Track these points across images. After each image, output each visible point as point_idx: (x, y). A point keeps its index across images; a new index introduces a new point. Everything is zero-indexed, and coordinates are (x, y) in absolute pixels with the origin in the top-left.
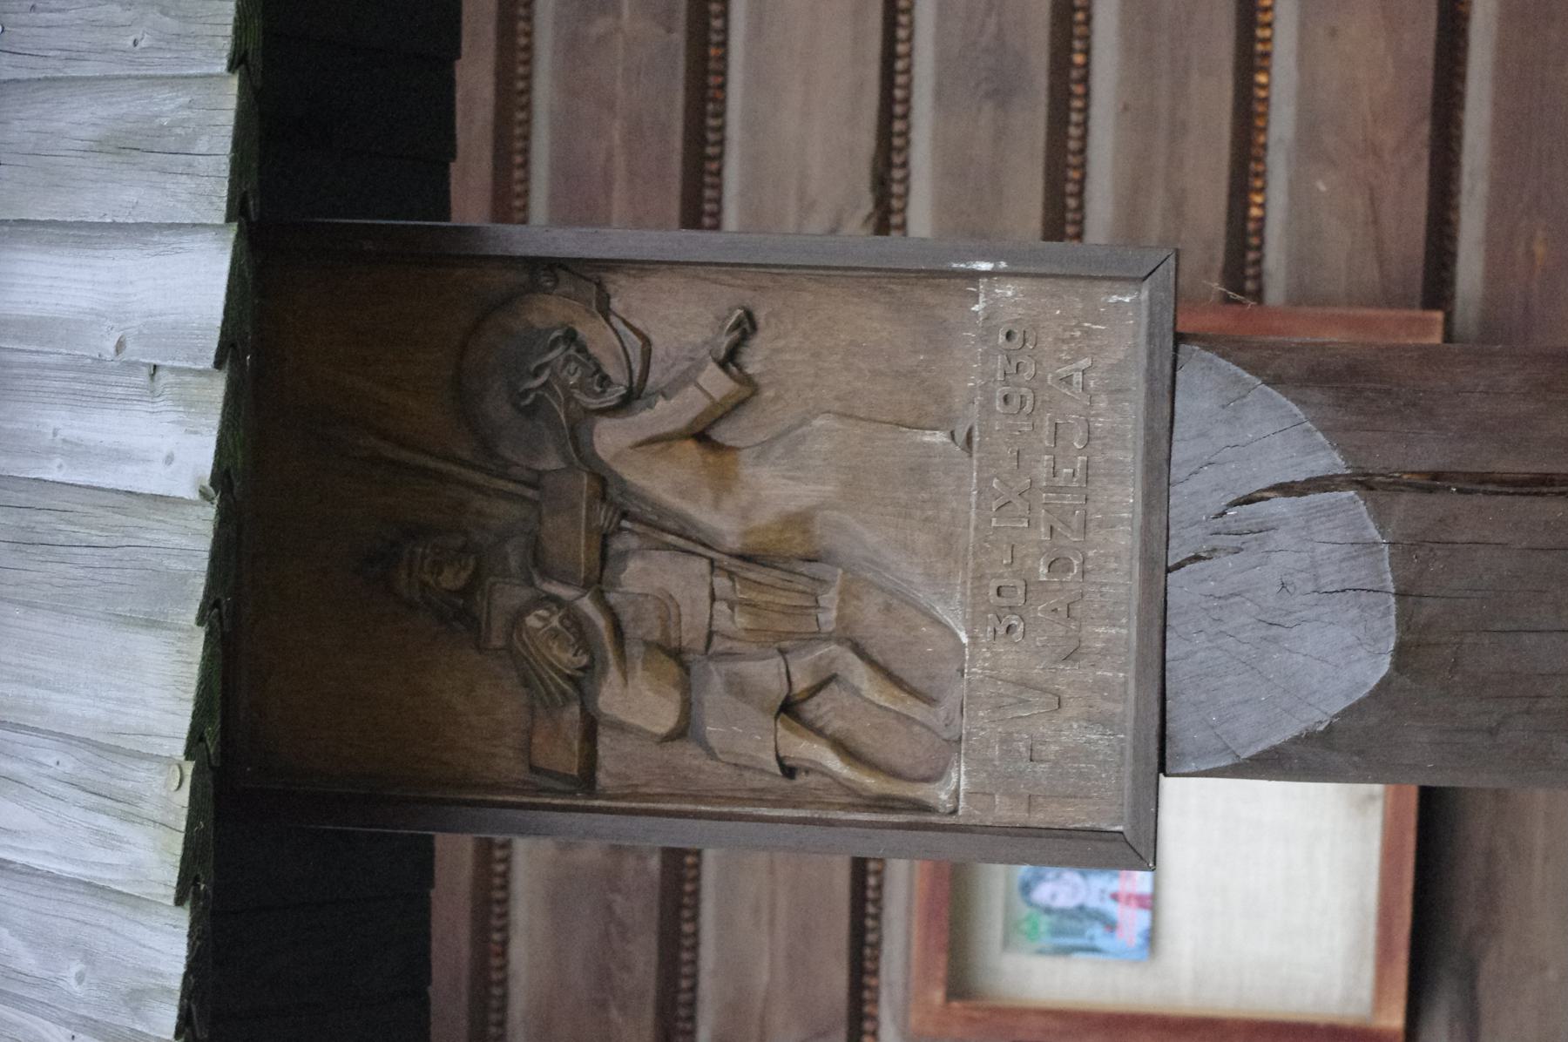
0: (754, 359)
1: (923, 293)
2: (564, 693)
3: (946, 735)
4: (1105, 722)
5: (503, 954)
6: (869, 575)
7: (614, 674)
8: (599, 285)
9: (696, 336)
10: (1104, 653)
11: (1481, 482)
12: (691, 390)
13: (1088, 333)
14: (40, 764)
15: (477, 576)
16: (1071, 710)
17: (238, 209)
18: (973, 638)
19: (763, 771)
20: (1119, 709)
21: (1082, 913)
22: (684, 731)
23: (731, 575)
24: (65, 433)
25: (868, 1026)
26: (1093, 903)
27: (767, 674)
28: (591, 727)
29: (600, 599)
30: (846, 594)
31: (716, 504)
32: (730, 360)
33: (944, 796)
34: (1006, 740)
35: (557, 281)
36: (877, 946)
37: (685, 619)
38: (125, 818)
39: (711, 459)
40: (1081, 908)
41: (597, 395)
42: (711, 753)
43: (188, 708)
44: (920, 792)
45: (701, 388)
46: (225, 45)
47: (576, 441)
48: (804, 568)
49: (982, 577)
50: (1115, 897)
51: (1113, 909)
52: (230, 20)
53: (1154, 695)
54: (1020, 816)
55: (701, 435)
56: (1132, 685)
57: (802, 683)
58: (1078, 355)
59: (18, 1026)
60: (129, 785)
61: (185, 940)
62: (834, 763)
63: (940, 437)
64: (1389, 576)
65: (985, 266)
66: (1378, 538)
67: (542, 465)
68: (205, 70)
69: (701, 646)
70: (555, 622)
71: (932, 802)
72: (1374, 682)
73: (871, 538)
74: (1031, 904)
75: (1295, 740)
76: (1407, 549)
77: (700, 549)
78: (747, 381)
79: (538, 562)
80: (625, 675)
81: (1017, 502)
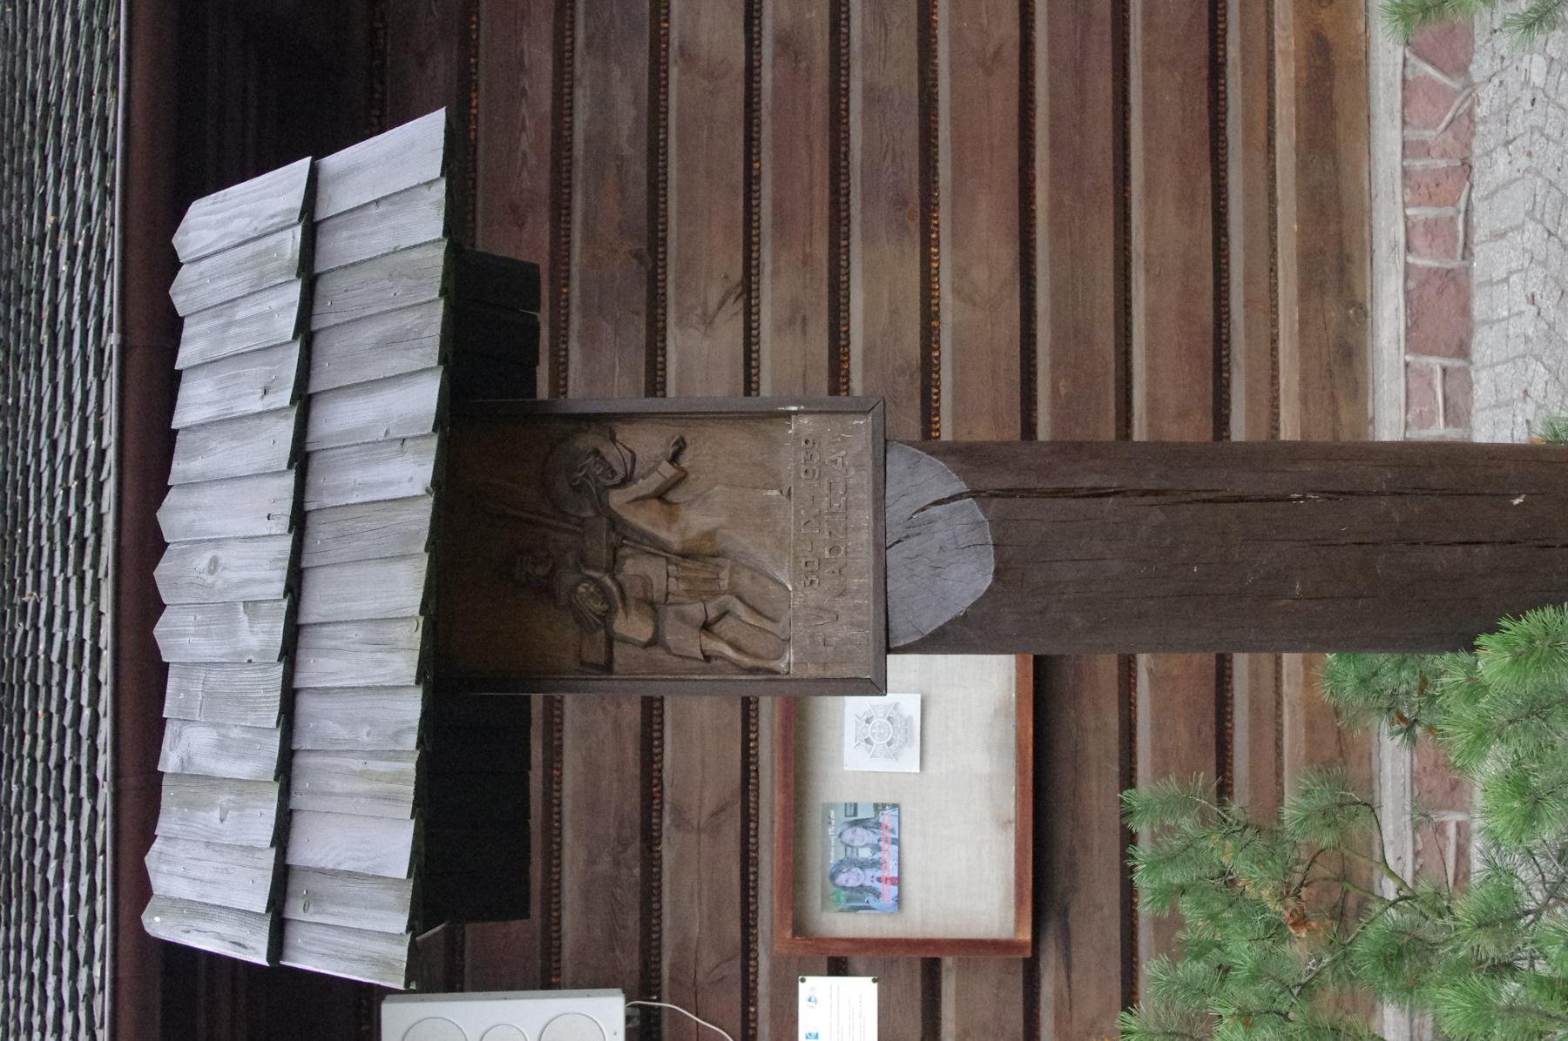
0: (685, 461)
1: (763, 426)
2: (596, 623)
3: (783, 637)
4: (860, 625)
5: (559, 924)
6: (743, 561)
7: (621, 613)
8: (610, 428)
9: (658, 451)
10: (858, 591)
11: (1027, 493)
12: (655, 475)
13: (844, 439)
14: (348, 638)
15: (552, 571)
16: (843, 619)
17: (443, 359)
18: (794, 587)
19: (696, 659)
20: (865, 618)
21: (862, 888)
22: (655, 641)
23: (677, 565)
24: (359, 481)
25: (752, 955)
26: (868, 883)
27: (695, 610)
28: (610, 640)
29: (613, 578)
30: (732, 570)
31: (669, 529)
32: (674, 459)
33: (783, 666)
34: (812, 636)
35: (589, 427)
36: (756, 912)
37: (655, 586)
38: (392, 651)
39: (665, 508)
40: (861, 886)
41: (608, 478)
42: (668, 650)
43: (421, 591)
44: (772, 664)
45: (660, 473)
46: (438, 286)
47: (602, 508)
48: (712, 560)
49: (797, 558)
50: (879, 880)
51: (876, 885)
52: (440, 274)
53: (882, 610)
54: (820, 673)
55: (660, 496)
56: (872, 607)
57: (712, 614)
58: (840, 449)
59: (338, 766)
60: (391, 636)
61: (420, 702)
62: (729, 652)
63: (775, 493)
64: (990, 537)
65: (794, 408)
66: (984, 518)
67: (584, 515)
68: (429, 298)
69: (662, 600)
70: (592, 589)
71: (777, 669)
72: (985, 588)
73: (744, 541)
74: (836, 886)
75: (951, 622)
76: (997, 524)
77: (662, 553)
78: (682, 470)
79: (583, 561)
80: (626, 614)
81: (813, 521)
